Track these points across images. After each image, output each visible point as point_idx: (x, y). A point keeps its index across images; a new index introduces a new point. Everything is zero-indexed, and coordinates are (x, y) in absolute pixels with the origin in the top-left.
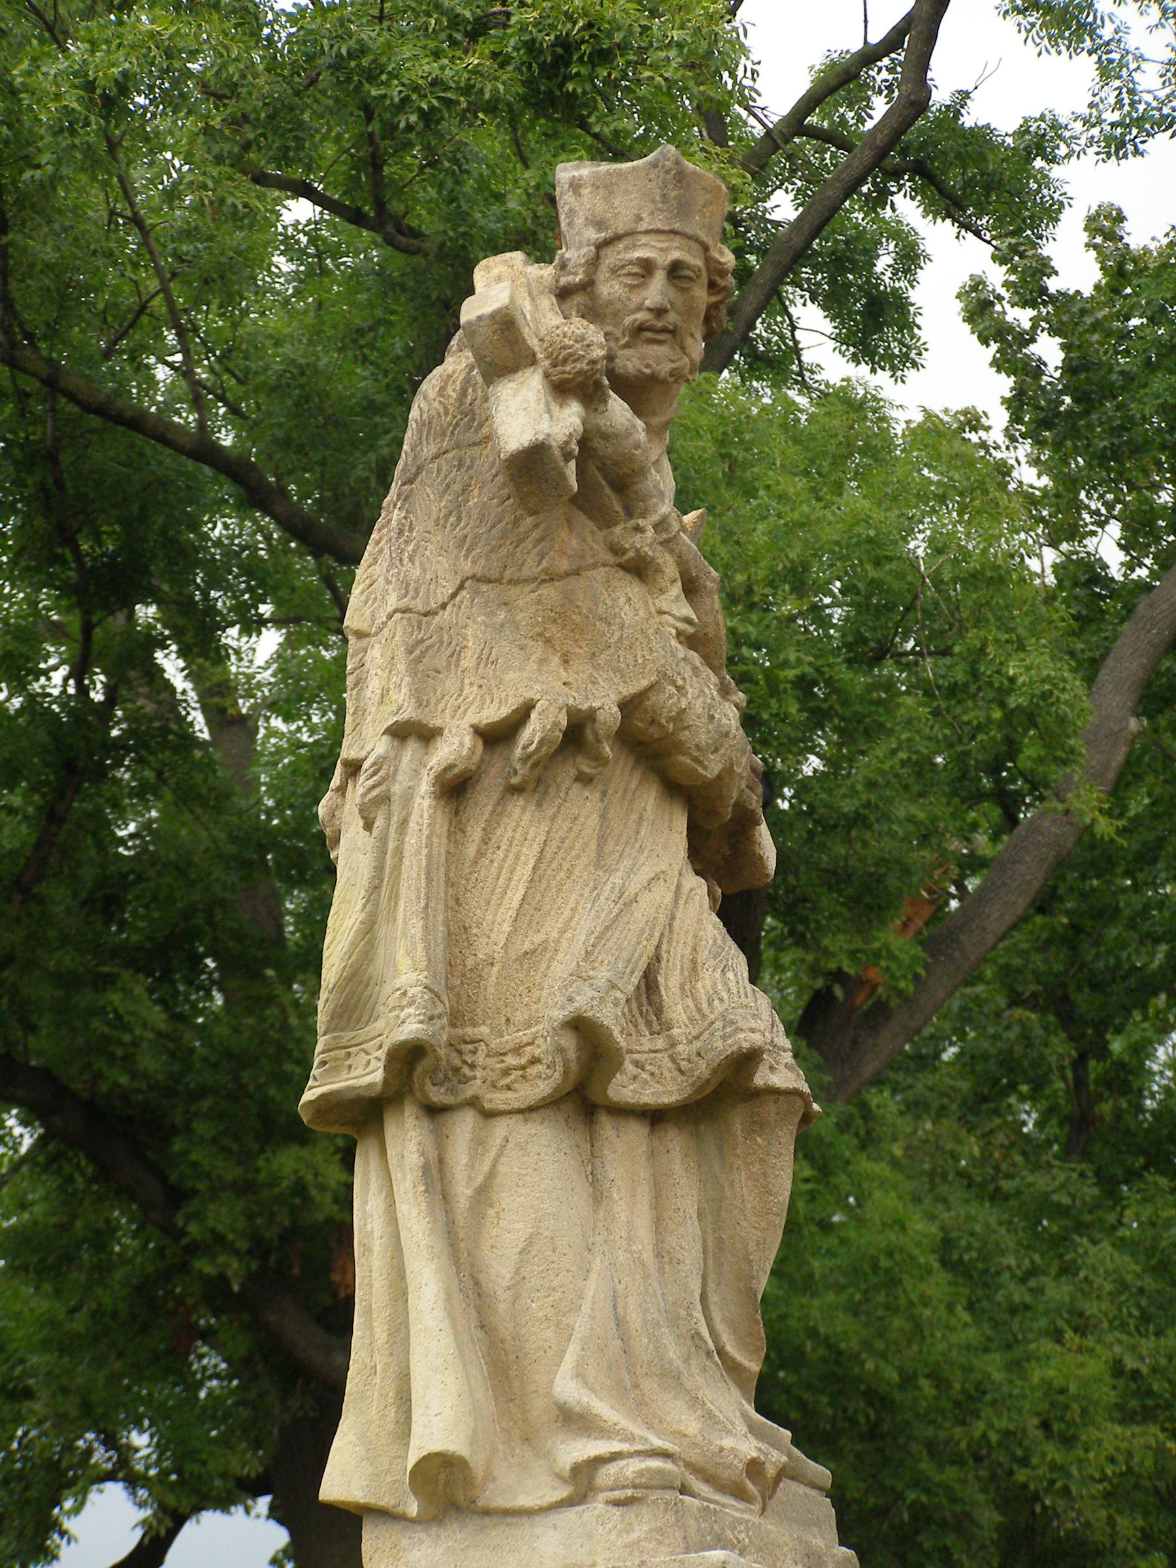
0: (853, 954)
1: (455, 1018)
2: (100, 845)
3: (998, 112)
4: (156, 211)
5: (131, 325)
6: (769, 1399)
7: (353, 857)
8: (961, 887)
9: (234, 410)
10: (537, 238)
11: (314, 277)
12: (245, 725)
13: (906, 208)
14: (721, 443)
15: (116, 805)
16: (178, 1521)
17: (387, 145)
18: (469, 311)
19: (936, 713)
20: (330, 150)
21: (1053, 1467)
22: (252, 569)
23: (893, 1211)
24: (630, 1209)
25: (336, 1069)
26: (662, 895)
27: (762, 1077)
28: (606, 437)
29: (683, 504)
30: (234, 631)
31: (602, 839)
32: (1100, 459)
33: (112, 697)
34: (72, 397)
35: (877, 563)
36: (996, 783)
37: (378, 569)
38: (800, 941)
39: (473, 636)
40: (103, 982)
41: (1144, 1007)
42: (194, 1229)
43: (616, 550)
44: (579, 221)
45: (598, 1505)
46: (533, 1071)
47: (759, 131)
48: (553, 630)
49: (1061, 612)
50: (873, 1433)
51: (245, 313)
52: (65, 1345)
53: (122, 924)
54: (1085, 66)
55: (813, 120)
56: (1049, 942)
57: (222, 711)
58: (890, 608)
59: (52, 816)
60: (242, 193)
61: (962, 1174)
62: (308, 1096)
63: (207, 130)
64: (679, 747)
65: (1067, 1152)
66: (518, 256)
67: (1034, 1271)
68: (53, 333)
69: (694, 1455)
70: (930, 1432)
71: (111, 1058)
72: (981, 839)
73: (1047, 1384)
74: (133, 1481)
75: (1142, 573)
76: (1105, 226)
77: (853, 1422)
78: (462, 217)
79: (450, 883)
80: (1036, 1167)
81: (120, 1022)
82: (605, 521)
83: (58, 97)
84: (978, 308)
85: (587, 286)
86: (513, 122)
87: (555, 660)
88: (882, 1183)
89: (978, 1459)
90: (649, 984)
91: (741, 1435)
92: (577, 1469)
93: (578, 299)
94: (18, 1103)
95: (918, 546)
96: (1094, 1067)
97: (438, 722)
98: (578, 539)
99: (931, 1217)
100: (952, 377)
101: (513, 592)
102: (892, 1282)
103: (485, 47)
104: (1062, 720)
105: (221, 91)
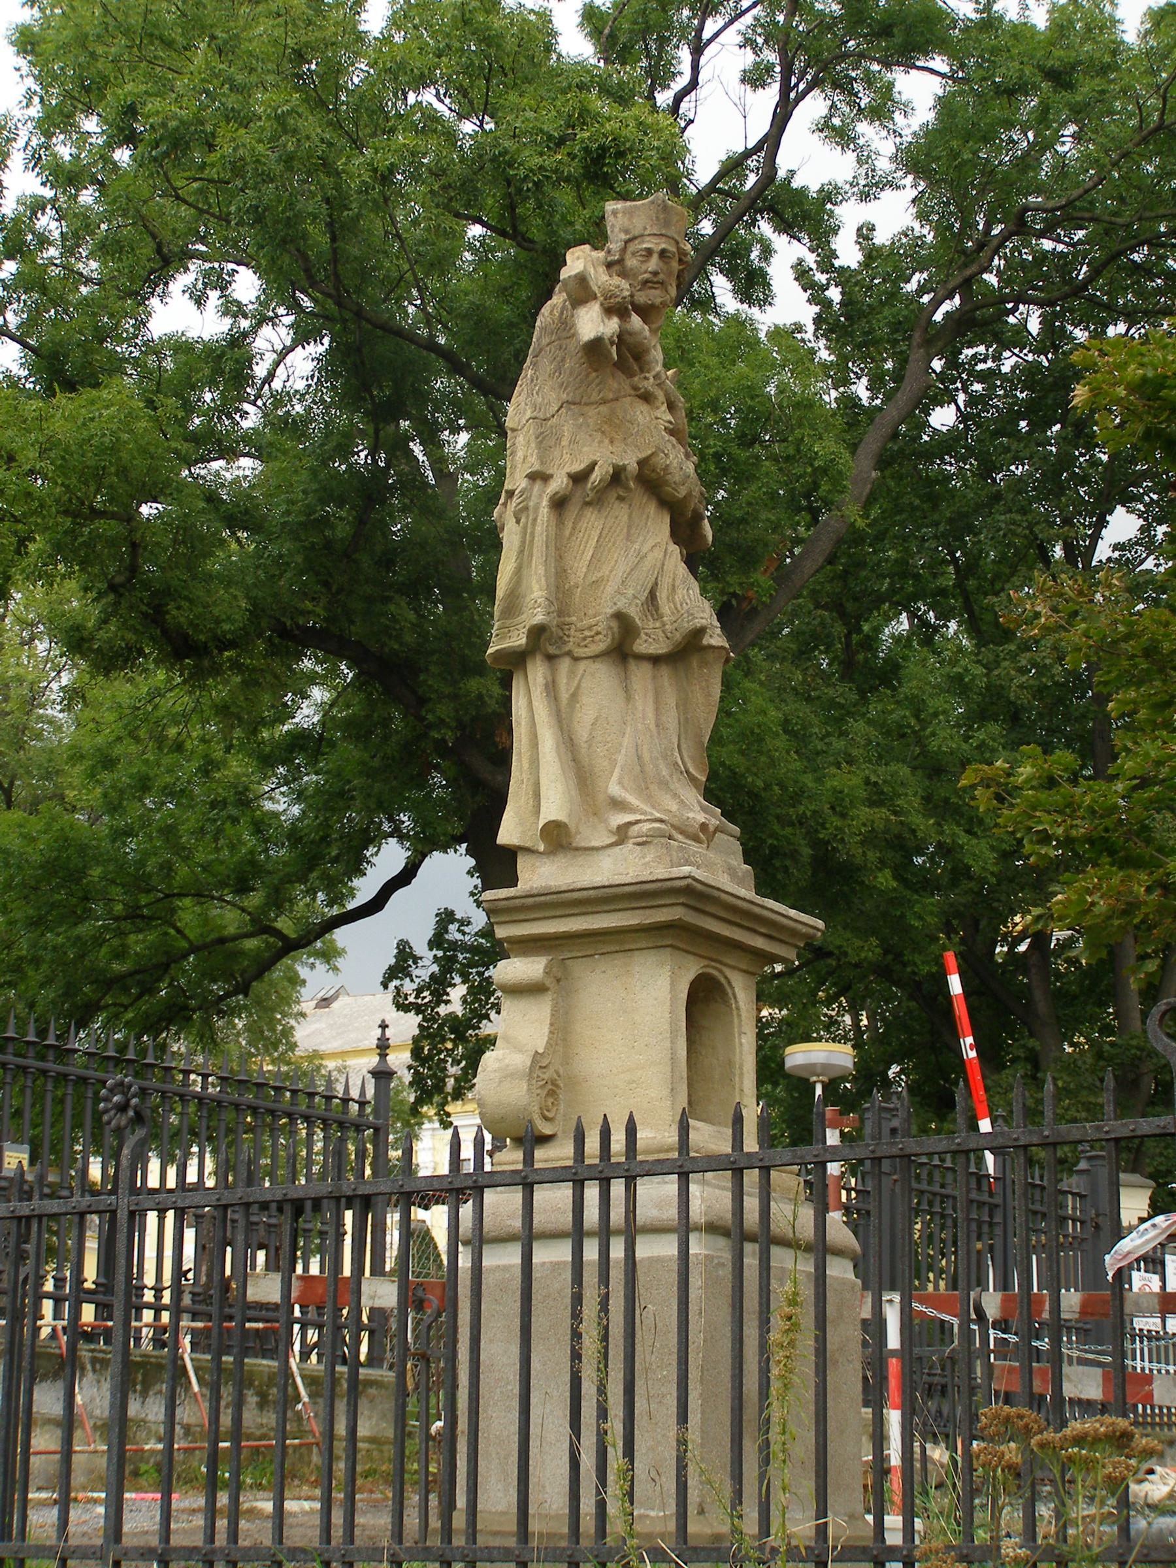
0: (741, 584)
1: (560, 613)
2: (385, 536)
3: (809, 179)
4: (407, 231)
5: (396, 286)
6: (711, 794)
7: (510, 537)
8: (792, 553)
9: (445, 326)
10: (596, 236)
11: (482, 261)
12: (452, 477)
13: (765, 227)
14: (677, 341)
15: (391, 515)
16: (424, 856)
17: (517, 199)
18: (565, 274)
19: (780, 469)
20: (490, 201)
21: (837, 828)
22: (455, 403)
23: (763, 708)
24: (644, 704)
25: (504, 638)
26: (658, 554)
27: (706, 641)
28: (630, 334)
29: (667, 367)
30: (447, 433)
31: (629, 527)
32: (859, 346)
33: (389, 465)
34: (368, 321)
35: (752, 398)
36: (808, 501)
37: (524, 396)
38: (715, 578)
39: (567, 431)
40: (387, 600)
41: (878, 609)
42: (430, 717)
43: (635, 388)
44: (616, 230)
45: (630, 845)
46: (597, 638)
47: (695, 191)
48: (605, 427)
49: (839, 421)
50: (751, 812)
51: (450, 280)
52: (370, 773)
53: (395, 572)
54: (851, 156)
55: (720, 185)
56: (833, 579)
57: (441, 471)
58: (758, 419)
59: (361, 521)
60: (448, 222)
61: (794, 689)
62: (490, 651)
63: (432, 192)
64: (666, 483)
65: (842, 678)
66: (587, 247)
67: (828, 734)
68: (359, 290)
69: (675, 821)
70: (778, 811)
71: (390, 636)
72: (801, 529)
73: (834, 788)
74: (402, 837)
75: (878, 402)
76: (865, 233)
77: (742, 806)
78: (554, 233)
79: (557, 549)
80: (828, 685)
81: (394, 619)
82: (630, 374)
83: (360, 175)
84: (801, 273)
85: (621, 261)
86: (578, 187)
87: (607, 441)
88: (756, 693)
89: (801, 824)
90: (652, 596)
91: (697, 811)
92: (619, 828)
93: (616, 268)
94: (346, 658)
95: (771, 389)
96: (855, 638)
97: (550, 472)
98: (616, 383)
99: (778, 709)
100: (789, 306)
101: (586, 409)
102: (761, 740)
103: (565, 150)
104: (840, 472)
105: (437, 172)
